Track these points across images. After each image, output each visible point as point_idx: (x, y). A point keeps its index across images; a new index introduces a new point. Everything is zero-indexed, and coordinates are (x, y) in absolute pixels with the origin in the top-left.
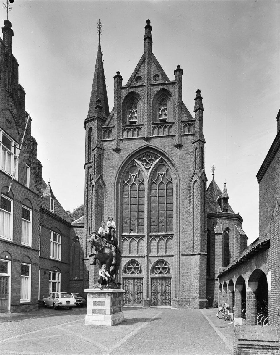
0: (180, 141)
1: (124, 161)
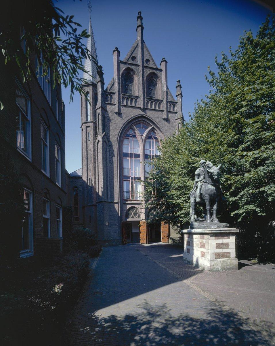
0: (168, 116)
1: (124, 124)
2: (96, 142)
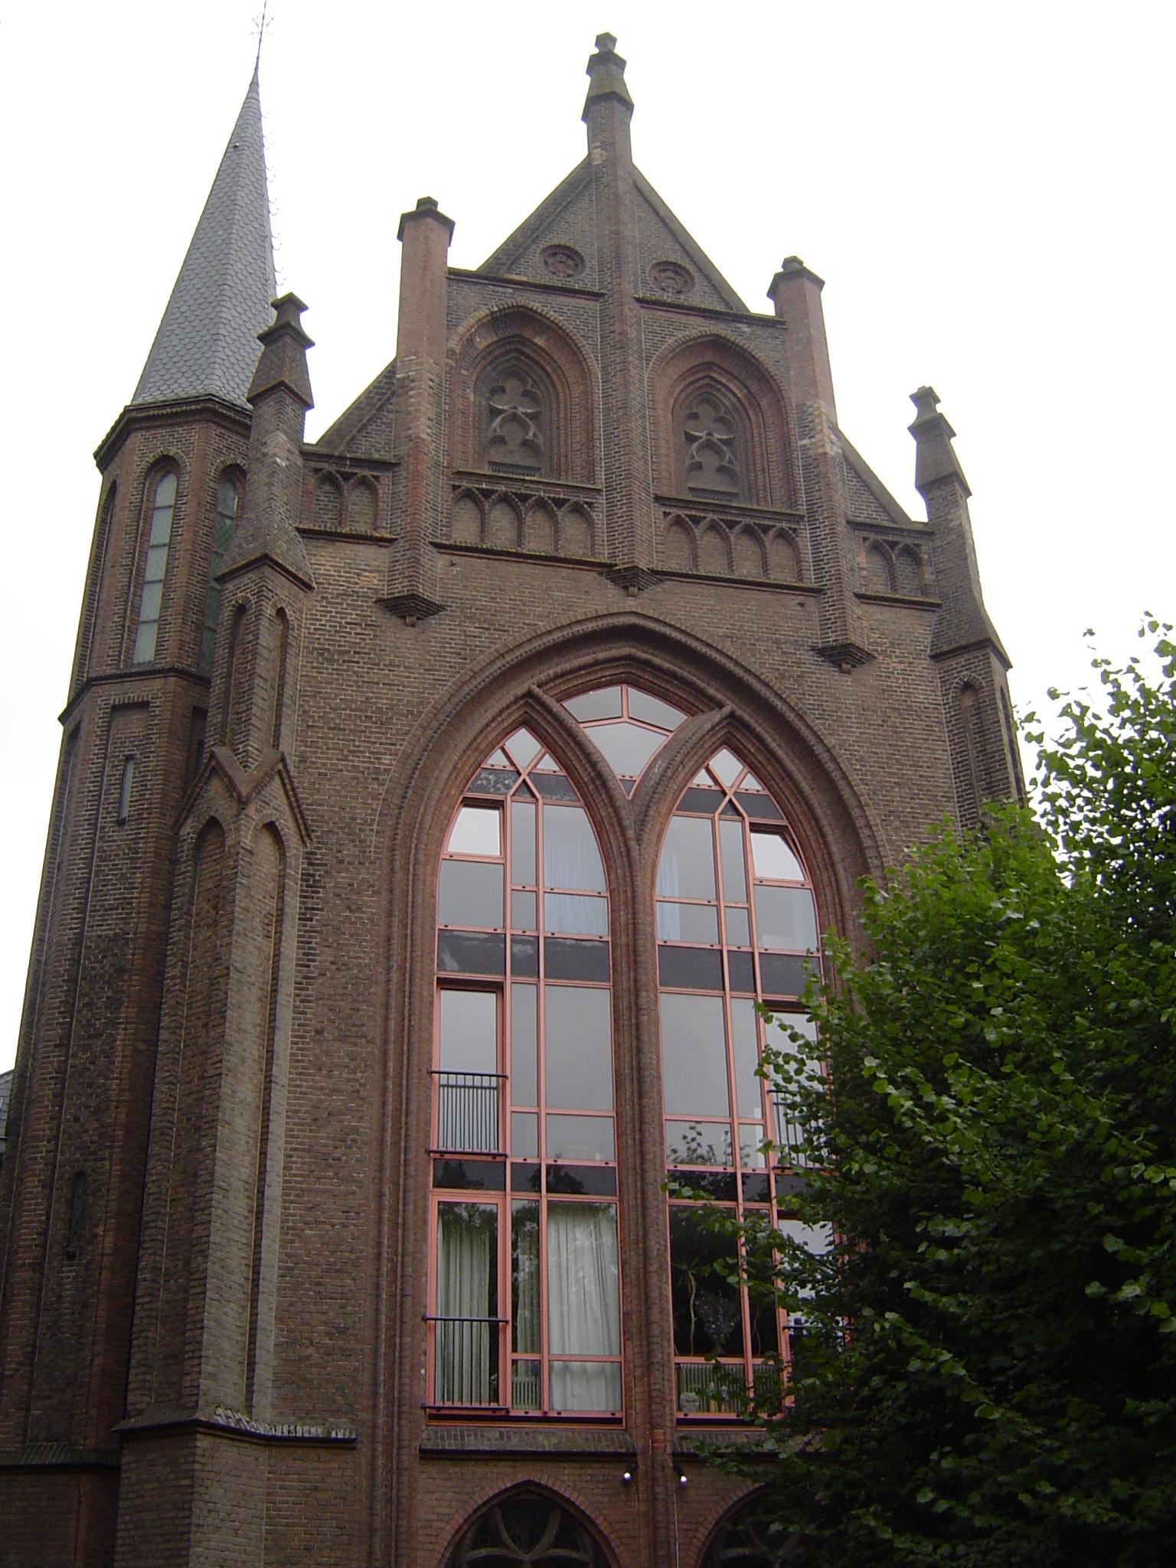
2: (189, 829)
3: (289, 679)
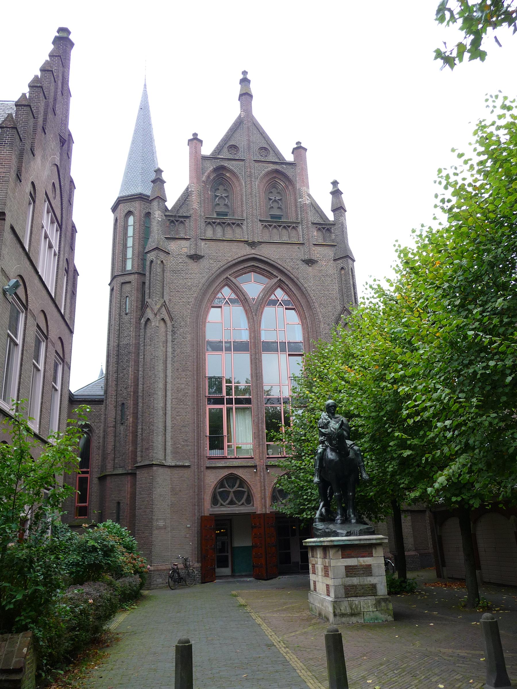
2: (143, 321)
3: (165, 280)
